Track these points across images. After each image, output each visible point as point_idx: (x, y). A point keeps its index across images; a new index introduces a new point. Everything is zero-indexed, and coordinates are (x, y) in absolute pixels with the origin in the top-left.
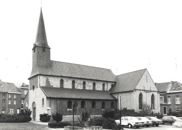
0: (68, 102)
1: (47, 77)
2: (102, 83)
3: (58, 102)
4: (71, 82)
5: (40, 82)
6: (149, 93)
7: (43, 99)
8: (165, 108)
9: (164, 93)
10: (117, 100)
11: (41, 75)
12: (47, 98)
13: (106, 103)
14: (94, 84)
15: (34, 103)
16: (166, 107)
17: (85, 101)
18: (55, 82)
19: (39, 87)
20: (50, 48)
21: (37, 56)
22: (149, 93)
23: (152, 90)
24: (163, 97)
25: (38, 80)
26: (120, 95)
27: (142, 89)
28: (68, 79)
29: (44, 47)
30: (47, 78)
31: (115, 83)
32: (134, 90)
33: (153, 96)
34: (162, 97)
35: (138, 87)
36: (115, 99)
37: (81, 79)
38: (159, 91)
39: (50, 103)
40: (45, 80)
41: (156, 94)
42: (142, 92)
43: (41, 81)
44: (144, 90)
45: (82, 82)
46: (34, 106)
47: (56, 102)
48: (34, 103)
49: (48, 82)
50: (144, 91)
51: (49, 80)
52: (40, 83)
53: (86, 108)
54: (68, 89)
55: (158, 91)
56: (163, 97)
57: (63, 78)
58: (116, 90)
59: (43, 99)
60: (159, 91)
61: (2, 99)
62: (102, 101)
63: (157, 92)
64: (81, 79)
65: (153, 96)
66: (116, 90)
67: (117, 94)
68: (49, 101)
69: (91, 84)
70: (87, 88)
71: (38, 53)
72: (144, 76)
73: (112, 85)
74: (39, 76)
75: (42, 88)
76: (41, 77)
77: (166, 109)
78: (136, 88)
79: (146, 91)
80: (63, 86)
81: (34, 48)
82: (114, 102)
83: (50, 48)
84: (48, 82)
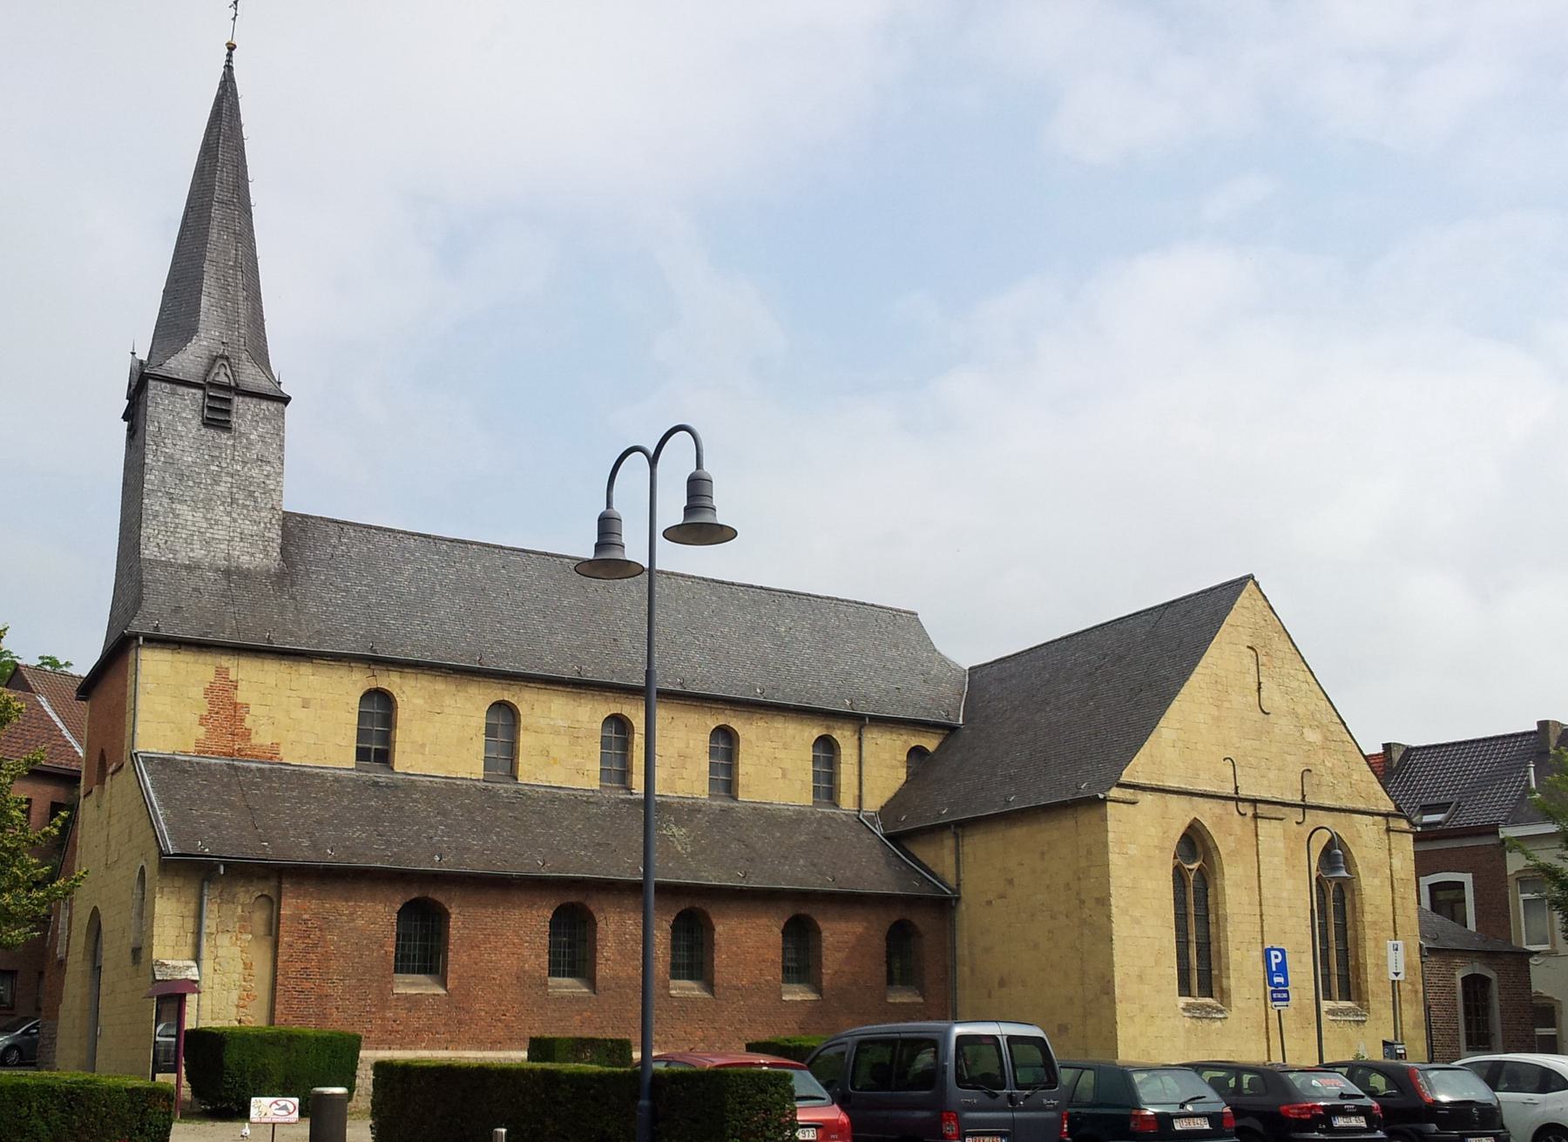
0: (555, 924)
1: (226, 661)
2: (802, 737)
4: (479, 719)
9: (1468, 843)
10: (944, 904)
15: (95, 914)
16: (1491, 974)
17: (592, 906)
18: (301, 714)
20: (285, 400)
24: (1467, 879)
28: (440, 685)
29: (221, 387)
30: (221, 673)
33: (1334, 855)
34: (1460, 885)
36: (927, 892)
40: (197, 693)
48: (95, 914)
51: (241, 696)
53: (603, 971)
55: (1391, 807)
56: (1467, 879)
57: (390, 681)
61: (89, 875)
62: (788, 911)
63: (1386, 815)
65: (1334, 855)
67: (949, 843)
73: (916, 753)
77: (1486, 998)
83: (285, 400)
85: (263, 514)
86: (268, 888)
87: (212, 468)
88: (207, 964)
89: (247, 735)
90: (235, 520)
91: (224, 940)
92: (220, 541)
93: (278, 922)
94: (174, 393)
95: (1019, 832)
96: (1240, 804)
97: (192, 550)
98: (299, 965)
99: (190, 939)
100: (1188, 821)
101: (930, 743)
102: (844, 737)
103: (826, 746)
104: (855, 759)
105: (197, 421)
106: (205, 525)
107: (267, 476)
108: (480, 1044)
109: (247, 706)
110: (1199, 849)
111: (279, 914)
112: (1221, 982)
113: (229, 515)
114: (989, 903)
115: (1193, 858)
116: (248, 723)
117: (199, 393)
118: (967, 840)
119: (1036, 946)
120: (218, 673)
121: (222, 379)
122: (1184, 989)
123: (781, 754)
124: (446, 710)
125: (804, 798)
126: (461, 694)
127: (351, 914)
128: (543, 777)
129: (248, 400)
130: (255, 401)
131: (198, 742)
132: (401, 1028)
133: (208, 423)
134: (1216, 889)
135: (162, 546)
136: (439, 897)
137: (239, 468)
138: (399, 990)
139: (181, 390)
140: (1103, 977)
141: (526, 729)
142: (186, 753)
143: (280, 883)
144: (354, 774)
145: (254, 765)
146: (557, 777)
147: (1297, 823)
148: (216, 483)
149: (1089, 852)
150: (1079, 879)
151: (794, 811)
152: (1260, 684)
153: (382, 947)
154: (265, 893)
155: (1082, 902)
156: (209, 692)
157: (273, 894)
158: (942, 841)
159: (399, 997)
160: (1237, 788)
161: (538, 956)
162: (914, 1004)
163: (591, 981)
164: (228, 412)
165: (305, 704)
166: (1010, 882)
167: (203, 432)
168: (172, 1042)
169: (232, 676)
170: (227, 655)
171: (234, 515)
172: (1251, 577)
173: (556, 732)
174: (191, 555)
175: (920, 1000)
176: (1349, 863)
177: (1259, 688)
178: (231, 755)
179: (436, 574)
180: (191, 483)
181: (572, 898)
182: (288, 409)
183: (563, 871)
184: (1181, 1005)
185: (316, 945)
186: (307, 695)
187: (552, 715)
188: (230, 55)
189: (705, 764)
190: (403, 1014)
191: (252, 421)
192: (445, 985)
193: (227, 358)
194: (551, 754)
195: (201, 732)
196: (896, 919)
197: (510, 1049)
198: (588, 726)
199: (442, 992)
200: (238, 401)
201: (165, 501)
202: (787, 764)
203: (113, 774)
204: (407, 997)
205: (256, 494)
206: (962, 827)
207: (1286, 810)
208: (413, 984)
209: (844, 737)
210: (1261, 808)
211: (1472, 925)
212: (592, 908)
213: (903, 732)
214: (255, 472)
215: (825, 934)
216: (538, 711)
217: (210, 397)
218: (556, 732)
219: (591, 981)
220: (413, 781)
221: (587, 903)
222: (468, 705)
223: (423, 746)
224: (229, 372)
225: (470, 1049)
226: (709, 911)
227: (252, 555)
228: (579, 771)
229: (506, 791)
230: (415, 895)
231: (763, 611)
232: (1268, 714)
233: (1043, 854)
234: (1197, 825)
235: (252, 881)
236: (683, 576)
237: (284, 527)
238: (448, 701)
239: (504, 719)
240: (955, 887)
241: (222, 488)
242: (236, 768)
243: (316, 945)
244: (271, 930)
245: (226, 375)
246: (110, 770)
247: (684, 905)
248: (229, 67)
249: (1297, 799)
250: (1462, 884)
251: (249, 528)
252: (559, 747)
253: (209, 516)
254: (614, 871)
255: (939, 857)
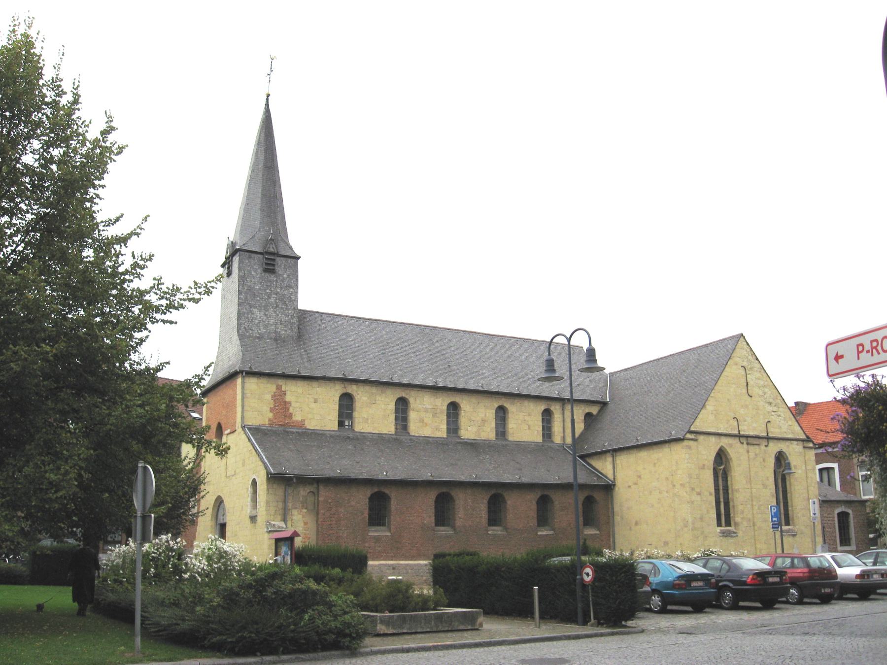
1: (280, 382)
3: (325, 493)
4: (392, 406)
5: (564, 421)
6: (763, 447)
7: (254, 483)
8: (843, 517)
10: (608, 488)
11: (251, 374)
12: (275, 479)
13: (394, 504)
14: (502, 414)
15: (219, 502)
16: (850, 511)
17: (453, 493)
18: (313, 405)
19: (239, 430)
20: (298, 258)
21: (240, 292)
22: (763, 447)
23: (774, 432)
24: (835, 466)
25: (239, 397)
26: (623, 460)
27: (729, 431)
28: (374, 390)
30: (279, 387)
31: (604, 404)
32: (689, 436)
33: (781, 459)
35: (705, 421)
37: (436, 389)
38: (808, 439)
39: (285, 502)
40: (268, 397)
41: (795, 454)
42: (725, 442)
43: (251, 402)
44: (739, 436)
45: (441, 402)
46: (220, 517)
47: (311, 499)
49: (281, 405)
50: (737, 440)
51: (288, 398)
52: (564, 421)
53: (459, 523)
54: (428, 442)
56: (835, 466)
57: (352, 389)
58: (603, 441)
59: (254, 483)
60: (808, 437)
62: (538, 494)
63: (803, 441)
64: (436, 389)
65: (781, 459)
66: (603, 441)
68: (280, 491)
69: (386, 403)
70: (468, 432)
71: (242, 279)
72: (732, 371)
73: (588, 415)
74: (239, 381)
75: (257, 433)
76: (252, 383)
77: (848, 522)
78: (698, 426)
79: (747, 437)
80: (405, 428)
81: (227, 258)
82: (598, 496)
83: (298, 258)
84: (281, 405)
85: (290, 312)
86: (312, 488)
87: (268, 291)
88: (289, 523)
89: (290, 416)
90: (278, 315)
91: (295, 512)
92: (271, 325)
93: (318, 504)
94: (250, 257)
95: (643, 454)
96: (741, 439)
97: (260, 330)
98: (328, 523)
99: (281, 512)
100: (718, 447)
101: (594, 410)
102: (556, 408)
103: (547, 415)
104: (561, 419)
105: (259, 271)
106: (265, 318)
107: (291, 294)
108: (406, 559)
109: (290, 403)
110: (724, 459)
111: (318, 499)
112: (734, 520)
113: (275, 312)
114: (629, 487)
115: (721, 464)
116: (291, 410)
117: (261, 256)
118: (618, 458)
119: (653, 506)
120: (277, 388)
121: (271, 250)
122: (719, 524)
123: (526, 418)
124: (377, 402)
125: (539, 439)
126: (384, 395)
127: (349, 499)
128: (421, 432)
129: (282, 258)
130: (285, 259)
131: (269, 419)
132: (372, 551)
133: (266, 270)
134: (731, 477)
135: (247, 328)
136: (387, 491)
137: (279, 291)
138: (371, 534)
139: (253, 255)
140: (685, 520)
141: (413, 410)
142: (264, 425)
143: (318, 486)
144: (338, 433)
145: (294, 430)
146: (427, 432)
147: (766, 446)
148: (269, 298)
149: (677, 463)
150: (672, 475)
151: (535, 445)
152: (747, 383)
153: (362, 514)
154: (312, 490)
155: (674, 486)
156: (274, 396)
157: (315, 491)
158: (606, 458)
159: (372, 537)
160: (739, 431)
161: (430, 517)
162: (596, 534)
163: (453, 527)
164: (274, 265)
165: (316, 401)
166: (640, 477)
167: (263, 275)
168: (373, 560)
169: (284, 388)
170: (280, 379)
171: (278, 313)
172: (742, 335)
173: (426, 411)
174: (259, 332)
175: (598, 532)
176: (788, 466)
177: (747, 385)
178: (284, 425)
179: (366, 337)
180: (258, 299)
181: (444, 490)
182: (299, 261)
183: (440, 478)
184: (718, 531)
185: (334, 514)
186: (316, 397)
187: (424, 403)
188: (267, 99)
189: (493, 425)
190: (373, 544)
191: (284, 268)
192: (390, 531)
193: (273, 240)
194: (425, 421)
195: (271, 415)
196: (586, 495)
197: (419, 560)
198: (441, 408)
199: (389, 534)
200: (278, 259)
201: (247, 307)
202: (530, 423)
203: (228, 434)
204: (374, 537)
205: (287, 302)
206: (615, 451)
207: (761, 440)
208: (376, 531)
209: (556, 408)
210: (751, 440)
211: (838, 488)
212: (453, 494)
213: (582, 406)
214: (286, 292)
215: (556, 503)
216: (418, 401)
217: (266, 258)
218: (426, 411)
219: (453, 527)
220: (364, 436)
221: (451, 492)
222: (387, 400)
223: (367, 419)
224: (274, 247)
225: (403, 560)
226: (504, 494)
227: (286, 331)
228: (437, 429)
229: (406, 439)
230: (376, 490)
231: (513, 349)
232: (751, 397)
233: (655, 464)
234: (723, 449)
235: (306, 485)
236: (475, 333)
237: (299, 318)
238: (378, 398)
239: (402, 405)
240: (613, 479)
241: (272, 300)
242: (287, 432)
243: (334, 514)
244: (315, 507)
245: (273, 248)
246: (226, 432)
247: (493, 492)
248: (267, 105)
249: (764, 434)
250: (833, 468)
251: (283, 317)
252: (428, 418)
253: (267, 313)
254: (462, 477)
255: (605, 466)
